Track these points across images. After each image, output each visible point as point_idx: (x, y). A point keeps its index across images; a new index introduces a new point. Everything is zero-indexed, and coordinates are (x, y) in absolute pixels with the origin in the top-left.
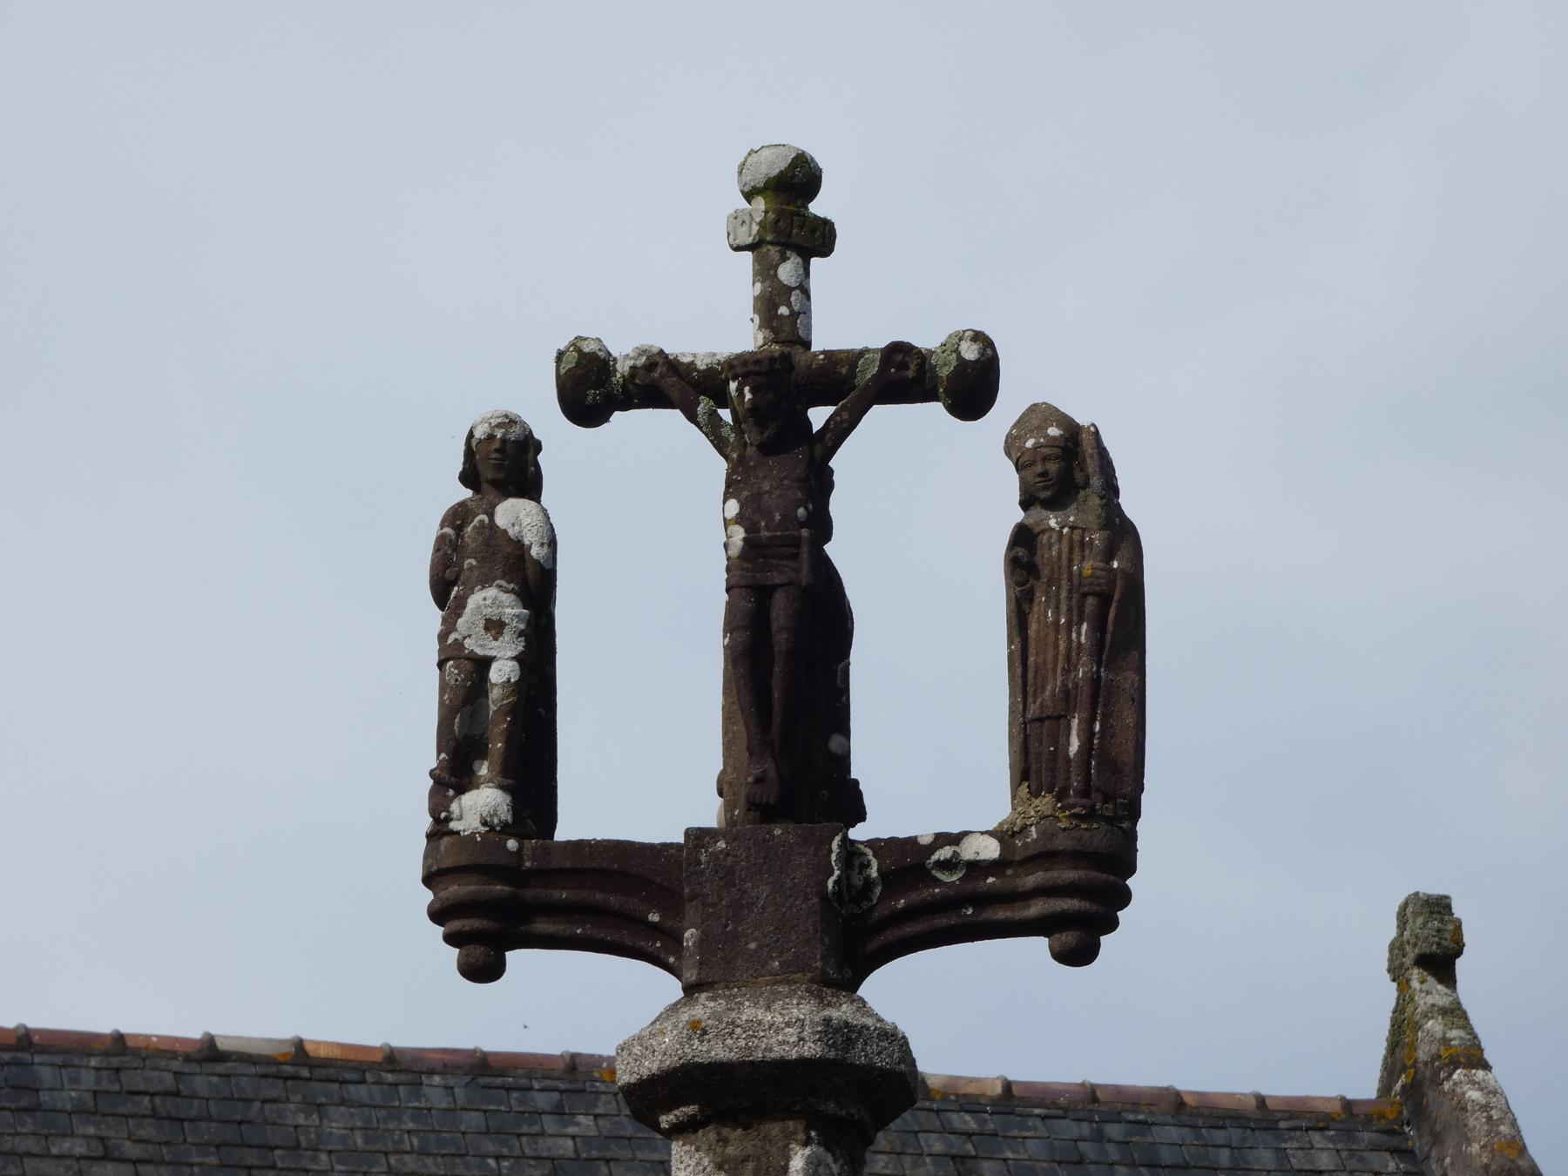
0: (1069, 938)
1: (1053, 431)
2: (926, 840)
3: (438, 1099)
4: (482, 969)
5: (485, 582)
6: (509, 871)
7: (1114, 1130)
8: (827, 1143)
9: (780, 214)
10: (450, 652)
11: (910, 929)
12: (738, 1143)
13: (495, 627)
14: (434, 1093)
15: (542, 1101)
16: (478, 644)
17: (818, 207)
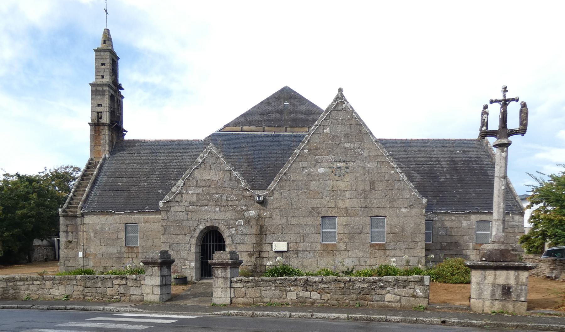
6: (486, 132)
10: (482, 119)
12: (501, 148)
13: (485, 117)
15: (427, 142)
17: (507, 89)
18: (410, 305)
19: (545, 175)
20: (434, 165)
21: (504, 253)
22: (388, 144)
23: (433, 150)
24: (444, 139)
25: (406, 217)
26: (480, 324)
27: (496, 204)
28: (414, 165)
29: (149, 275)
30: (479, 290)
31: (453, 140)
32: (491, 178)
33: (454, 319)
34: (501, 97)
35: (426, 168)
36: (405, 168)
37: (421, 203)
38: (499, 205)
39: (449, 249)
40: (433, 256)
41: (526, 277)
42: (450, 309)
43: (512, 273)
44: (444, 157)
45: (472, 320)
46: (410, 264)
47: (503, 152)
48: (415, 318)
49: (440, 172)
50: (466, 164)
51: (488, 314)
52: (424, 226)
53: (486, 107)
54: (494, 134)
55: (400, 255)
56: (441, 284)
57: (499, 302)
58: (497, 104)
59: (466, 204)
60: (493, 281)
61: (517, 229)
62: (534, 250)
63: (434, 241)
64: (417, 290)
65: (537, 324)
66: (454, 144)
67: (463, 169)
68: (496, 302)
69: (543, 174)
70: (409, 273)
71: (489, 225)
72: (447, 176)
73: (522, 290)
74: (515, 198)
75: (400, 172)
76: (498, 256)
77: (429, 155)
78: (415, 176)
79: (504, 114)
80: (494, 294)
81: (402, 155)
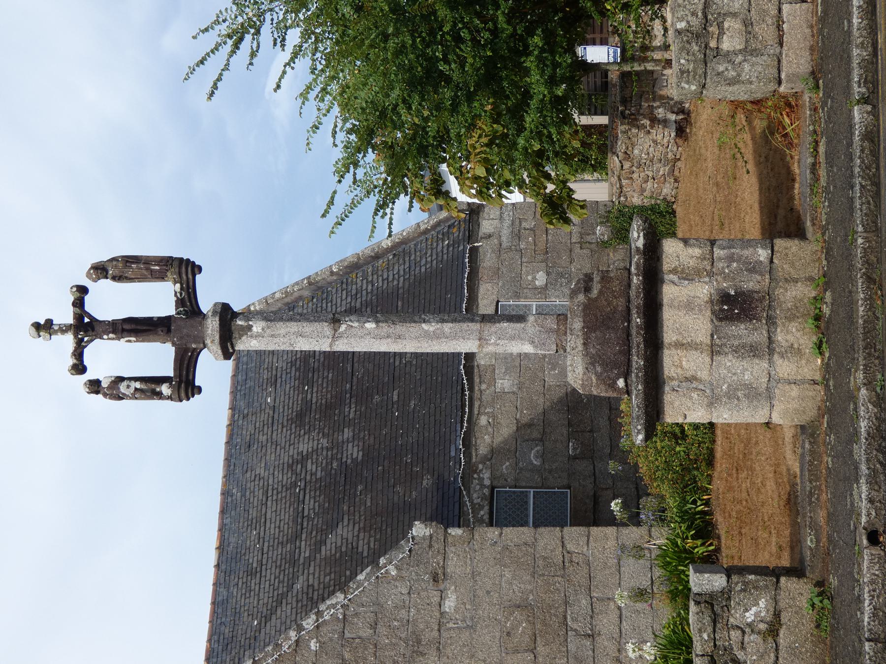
0: (196, 270)
1: (92, 271)
2: (176, 299)
3: (228, 520)
4: (199, 390)
5: (119, 389)
7: (239, 388)
8: (236, 318)
9: (44, 329)
11: (194, 302)
12: (235, 335)
13: (128, 387)
14: (228, 521)
15: (230, 499)
16: (132, 390)
17: (42, 322)
18: (808, 645)
19: (335, 192)
20: (308, 478)
21: (596, 316)
22: (227, 631)
23: (257, 478)
24: (227, 443)
25: (474, 596)
26: (871, 407)
27: (426, 345)
28: (303, 543)
29: (664, 35)
30: (738, 399)
31: (233, 416)
32: (359, 300)
33: (856, 497)
34: (68, 341)
35: (317, 504)
36: (311, 577)
37: (428, 542)
38: (427, 336)
39: (591, 431)
40: (616, 504)
41: (681, 245)
42: (818, 499)
43: (670, 292)
44: (283, 445)
45: (856, 433)
46: (645, 583)
47: (250, 328)
48: (867, 646)
49: (332, 459)
50: (310, 375)
51: (826, 367)
52: (507, 530)
53: (95, 386)
54: (187, 358)
55: (614, 616)
56: (716, 474)
57: (779, 330)
58: (89, 353)
59: (440, 378)
60: (701, 352)
61: (524, 224)
62: (593, 154)
63: (565, 482)
64: (749, 620)
65: (858, 214)
66: (246, 412)
67: (325, 385)
68: (780, 338)
69: (333, 198)
70: (681, 588)
71: (510, 305)
72: (346, 436)
73: (731, 259)
74: (426, 231)
75: (314, 617)
76: (611, 335)
77: (275, 492)
78: (339, 544)
79: (123, 330)
80: (751, 346)
81: (267, 583)
